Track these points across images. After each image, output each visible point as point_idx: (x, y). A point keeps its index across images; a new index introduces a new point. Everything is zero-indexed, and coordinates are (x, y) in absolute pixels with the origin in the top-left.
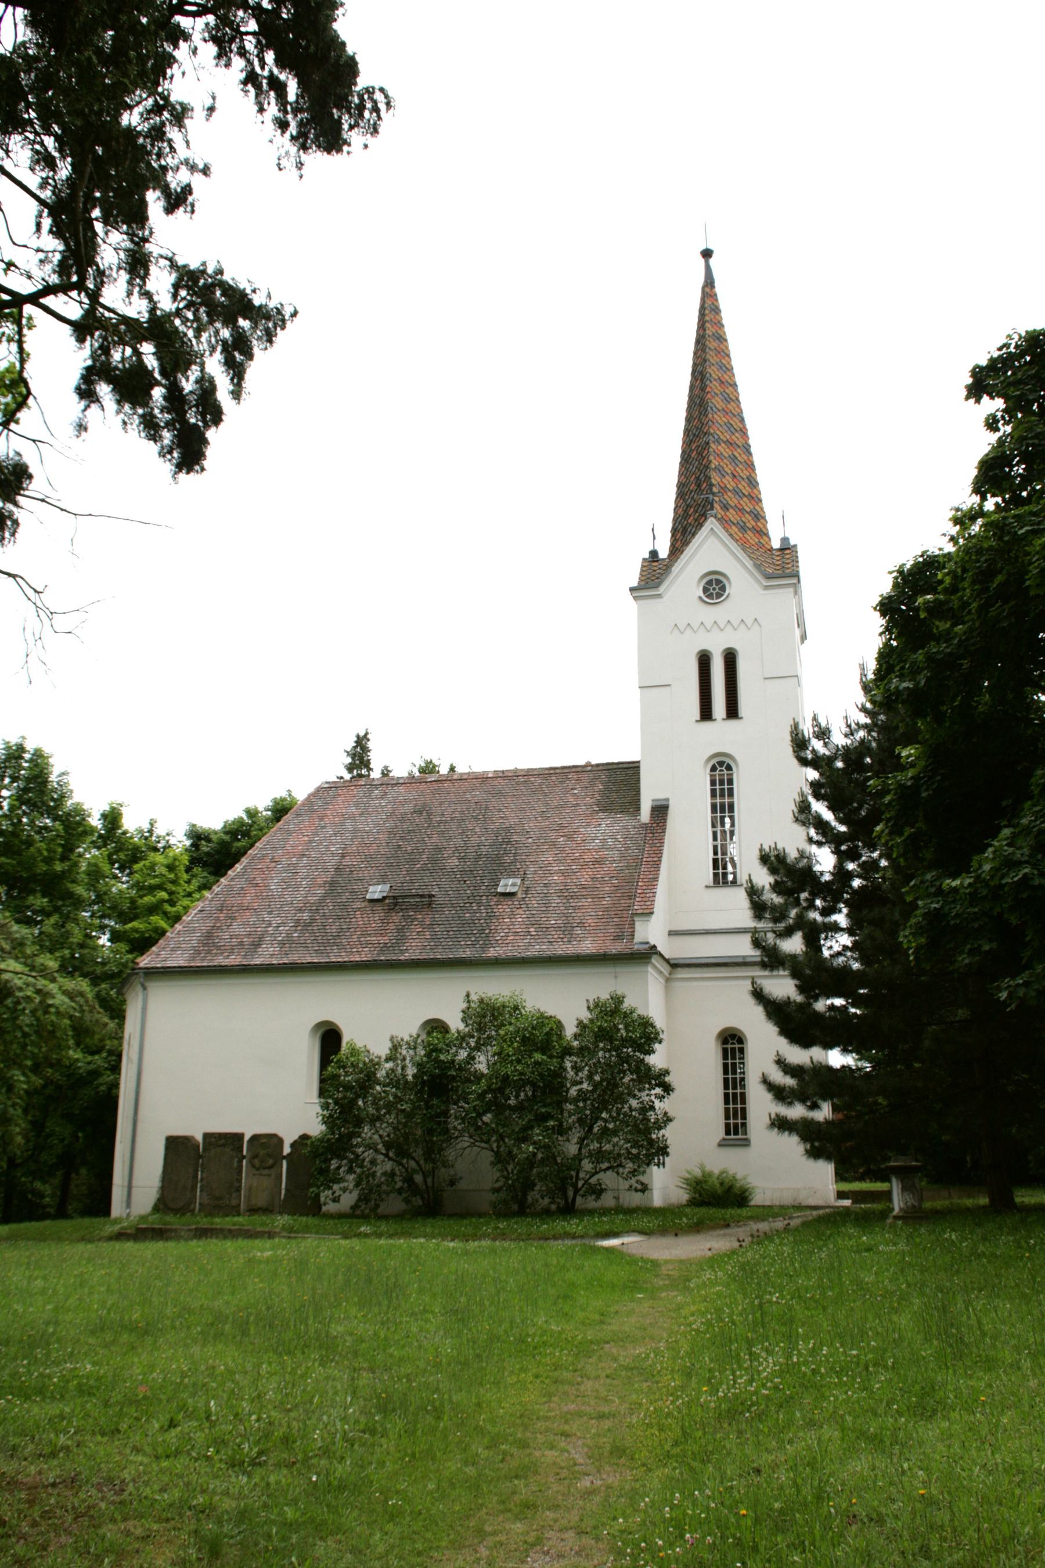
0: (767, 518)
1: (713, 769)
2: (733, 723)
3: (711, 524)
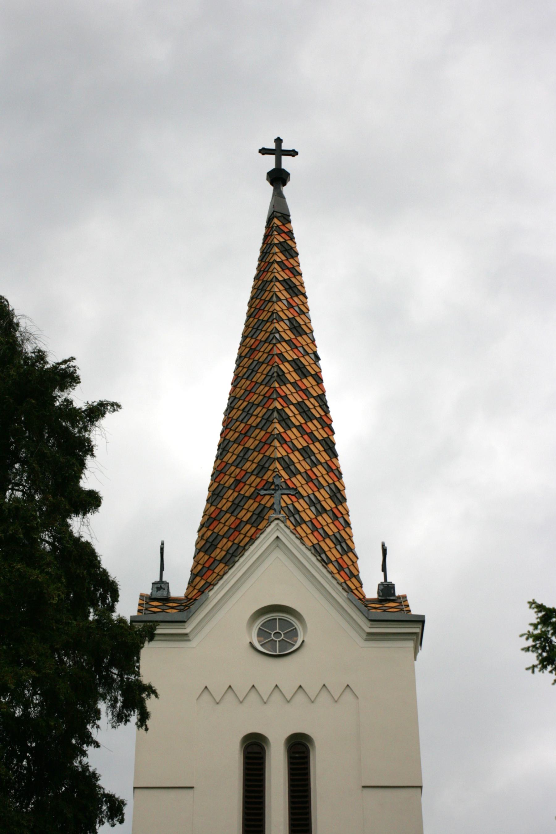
0: (357, 551)
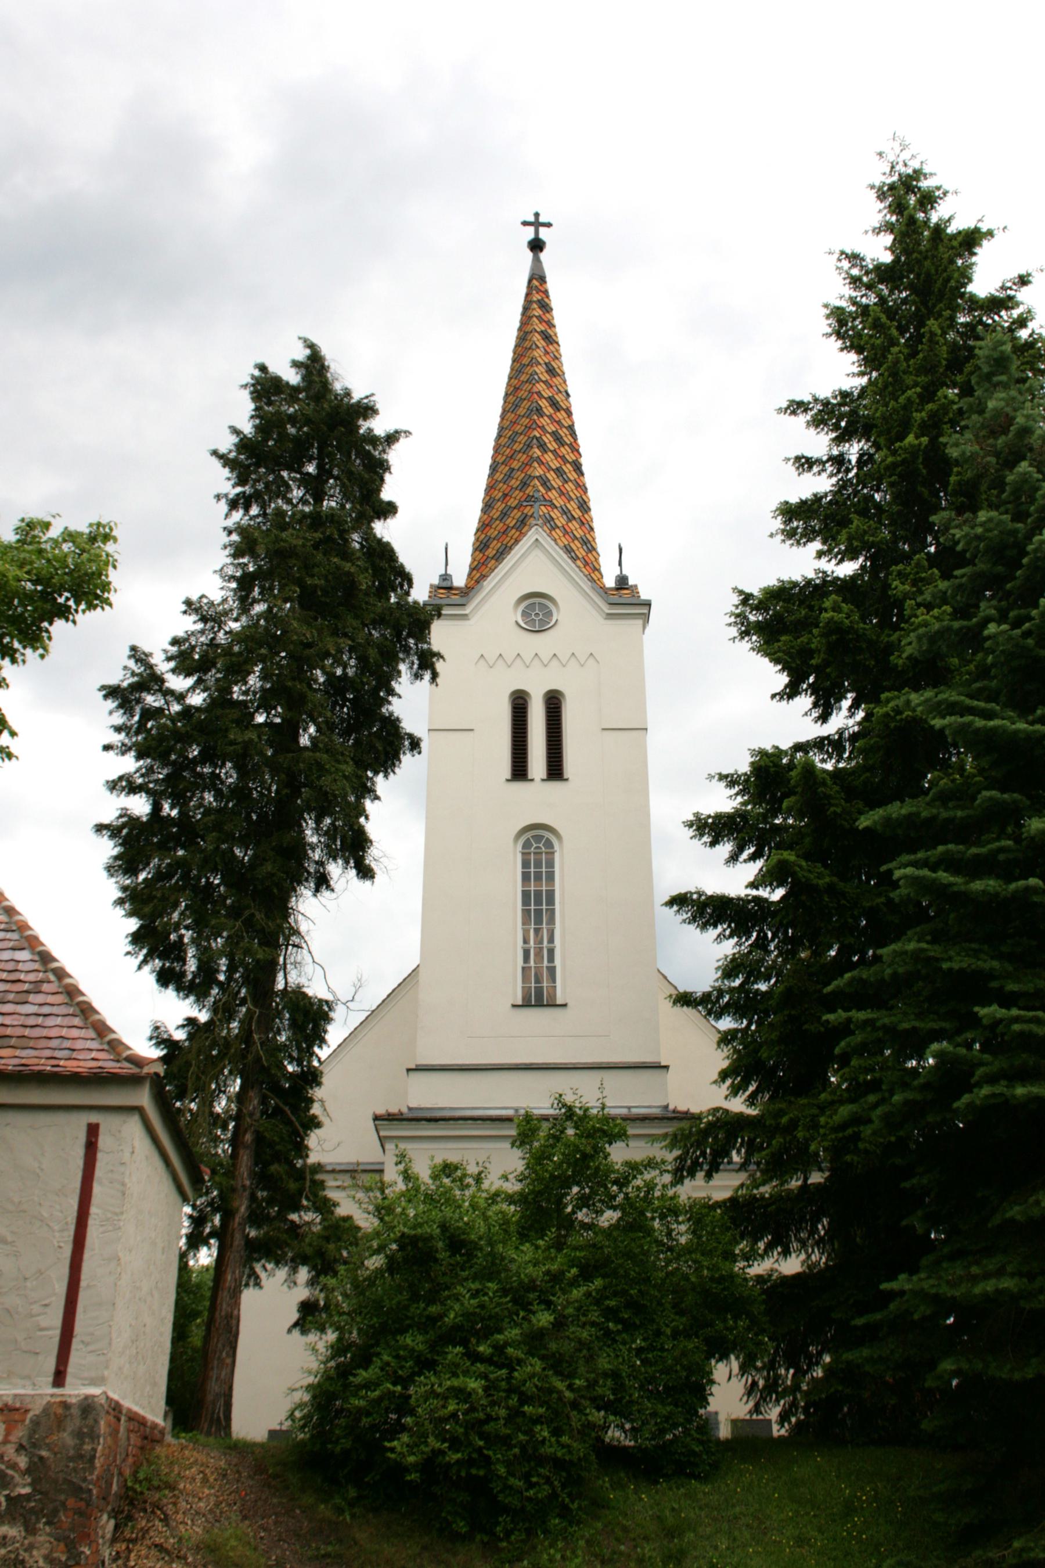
0: (599, 550)
1: (527, 845)
2: (555, 786)
3: (535, 534)
